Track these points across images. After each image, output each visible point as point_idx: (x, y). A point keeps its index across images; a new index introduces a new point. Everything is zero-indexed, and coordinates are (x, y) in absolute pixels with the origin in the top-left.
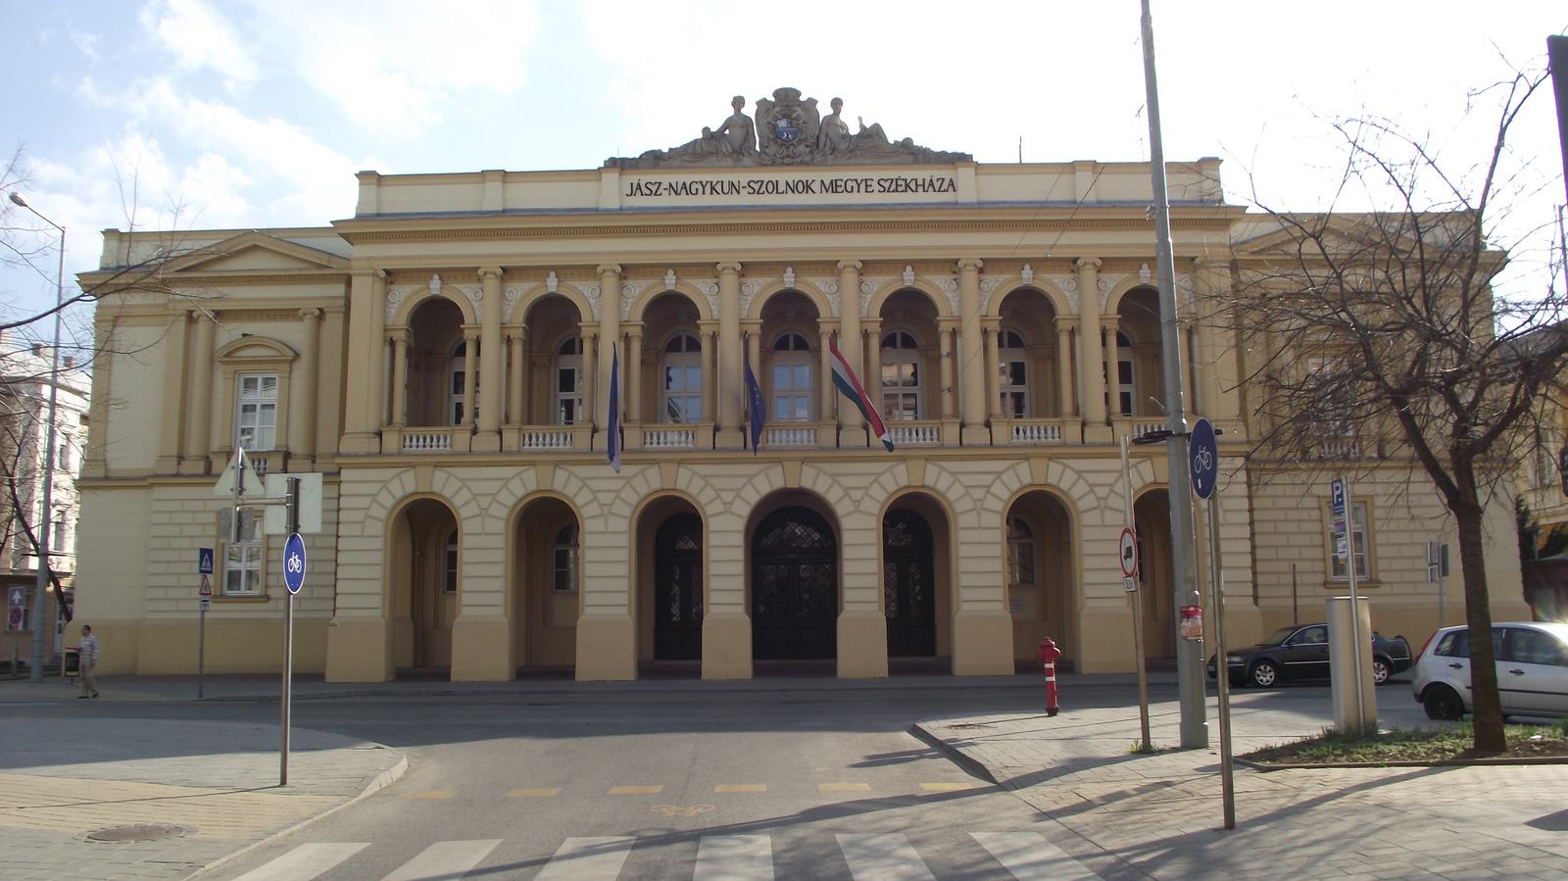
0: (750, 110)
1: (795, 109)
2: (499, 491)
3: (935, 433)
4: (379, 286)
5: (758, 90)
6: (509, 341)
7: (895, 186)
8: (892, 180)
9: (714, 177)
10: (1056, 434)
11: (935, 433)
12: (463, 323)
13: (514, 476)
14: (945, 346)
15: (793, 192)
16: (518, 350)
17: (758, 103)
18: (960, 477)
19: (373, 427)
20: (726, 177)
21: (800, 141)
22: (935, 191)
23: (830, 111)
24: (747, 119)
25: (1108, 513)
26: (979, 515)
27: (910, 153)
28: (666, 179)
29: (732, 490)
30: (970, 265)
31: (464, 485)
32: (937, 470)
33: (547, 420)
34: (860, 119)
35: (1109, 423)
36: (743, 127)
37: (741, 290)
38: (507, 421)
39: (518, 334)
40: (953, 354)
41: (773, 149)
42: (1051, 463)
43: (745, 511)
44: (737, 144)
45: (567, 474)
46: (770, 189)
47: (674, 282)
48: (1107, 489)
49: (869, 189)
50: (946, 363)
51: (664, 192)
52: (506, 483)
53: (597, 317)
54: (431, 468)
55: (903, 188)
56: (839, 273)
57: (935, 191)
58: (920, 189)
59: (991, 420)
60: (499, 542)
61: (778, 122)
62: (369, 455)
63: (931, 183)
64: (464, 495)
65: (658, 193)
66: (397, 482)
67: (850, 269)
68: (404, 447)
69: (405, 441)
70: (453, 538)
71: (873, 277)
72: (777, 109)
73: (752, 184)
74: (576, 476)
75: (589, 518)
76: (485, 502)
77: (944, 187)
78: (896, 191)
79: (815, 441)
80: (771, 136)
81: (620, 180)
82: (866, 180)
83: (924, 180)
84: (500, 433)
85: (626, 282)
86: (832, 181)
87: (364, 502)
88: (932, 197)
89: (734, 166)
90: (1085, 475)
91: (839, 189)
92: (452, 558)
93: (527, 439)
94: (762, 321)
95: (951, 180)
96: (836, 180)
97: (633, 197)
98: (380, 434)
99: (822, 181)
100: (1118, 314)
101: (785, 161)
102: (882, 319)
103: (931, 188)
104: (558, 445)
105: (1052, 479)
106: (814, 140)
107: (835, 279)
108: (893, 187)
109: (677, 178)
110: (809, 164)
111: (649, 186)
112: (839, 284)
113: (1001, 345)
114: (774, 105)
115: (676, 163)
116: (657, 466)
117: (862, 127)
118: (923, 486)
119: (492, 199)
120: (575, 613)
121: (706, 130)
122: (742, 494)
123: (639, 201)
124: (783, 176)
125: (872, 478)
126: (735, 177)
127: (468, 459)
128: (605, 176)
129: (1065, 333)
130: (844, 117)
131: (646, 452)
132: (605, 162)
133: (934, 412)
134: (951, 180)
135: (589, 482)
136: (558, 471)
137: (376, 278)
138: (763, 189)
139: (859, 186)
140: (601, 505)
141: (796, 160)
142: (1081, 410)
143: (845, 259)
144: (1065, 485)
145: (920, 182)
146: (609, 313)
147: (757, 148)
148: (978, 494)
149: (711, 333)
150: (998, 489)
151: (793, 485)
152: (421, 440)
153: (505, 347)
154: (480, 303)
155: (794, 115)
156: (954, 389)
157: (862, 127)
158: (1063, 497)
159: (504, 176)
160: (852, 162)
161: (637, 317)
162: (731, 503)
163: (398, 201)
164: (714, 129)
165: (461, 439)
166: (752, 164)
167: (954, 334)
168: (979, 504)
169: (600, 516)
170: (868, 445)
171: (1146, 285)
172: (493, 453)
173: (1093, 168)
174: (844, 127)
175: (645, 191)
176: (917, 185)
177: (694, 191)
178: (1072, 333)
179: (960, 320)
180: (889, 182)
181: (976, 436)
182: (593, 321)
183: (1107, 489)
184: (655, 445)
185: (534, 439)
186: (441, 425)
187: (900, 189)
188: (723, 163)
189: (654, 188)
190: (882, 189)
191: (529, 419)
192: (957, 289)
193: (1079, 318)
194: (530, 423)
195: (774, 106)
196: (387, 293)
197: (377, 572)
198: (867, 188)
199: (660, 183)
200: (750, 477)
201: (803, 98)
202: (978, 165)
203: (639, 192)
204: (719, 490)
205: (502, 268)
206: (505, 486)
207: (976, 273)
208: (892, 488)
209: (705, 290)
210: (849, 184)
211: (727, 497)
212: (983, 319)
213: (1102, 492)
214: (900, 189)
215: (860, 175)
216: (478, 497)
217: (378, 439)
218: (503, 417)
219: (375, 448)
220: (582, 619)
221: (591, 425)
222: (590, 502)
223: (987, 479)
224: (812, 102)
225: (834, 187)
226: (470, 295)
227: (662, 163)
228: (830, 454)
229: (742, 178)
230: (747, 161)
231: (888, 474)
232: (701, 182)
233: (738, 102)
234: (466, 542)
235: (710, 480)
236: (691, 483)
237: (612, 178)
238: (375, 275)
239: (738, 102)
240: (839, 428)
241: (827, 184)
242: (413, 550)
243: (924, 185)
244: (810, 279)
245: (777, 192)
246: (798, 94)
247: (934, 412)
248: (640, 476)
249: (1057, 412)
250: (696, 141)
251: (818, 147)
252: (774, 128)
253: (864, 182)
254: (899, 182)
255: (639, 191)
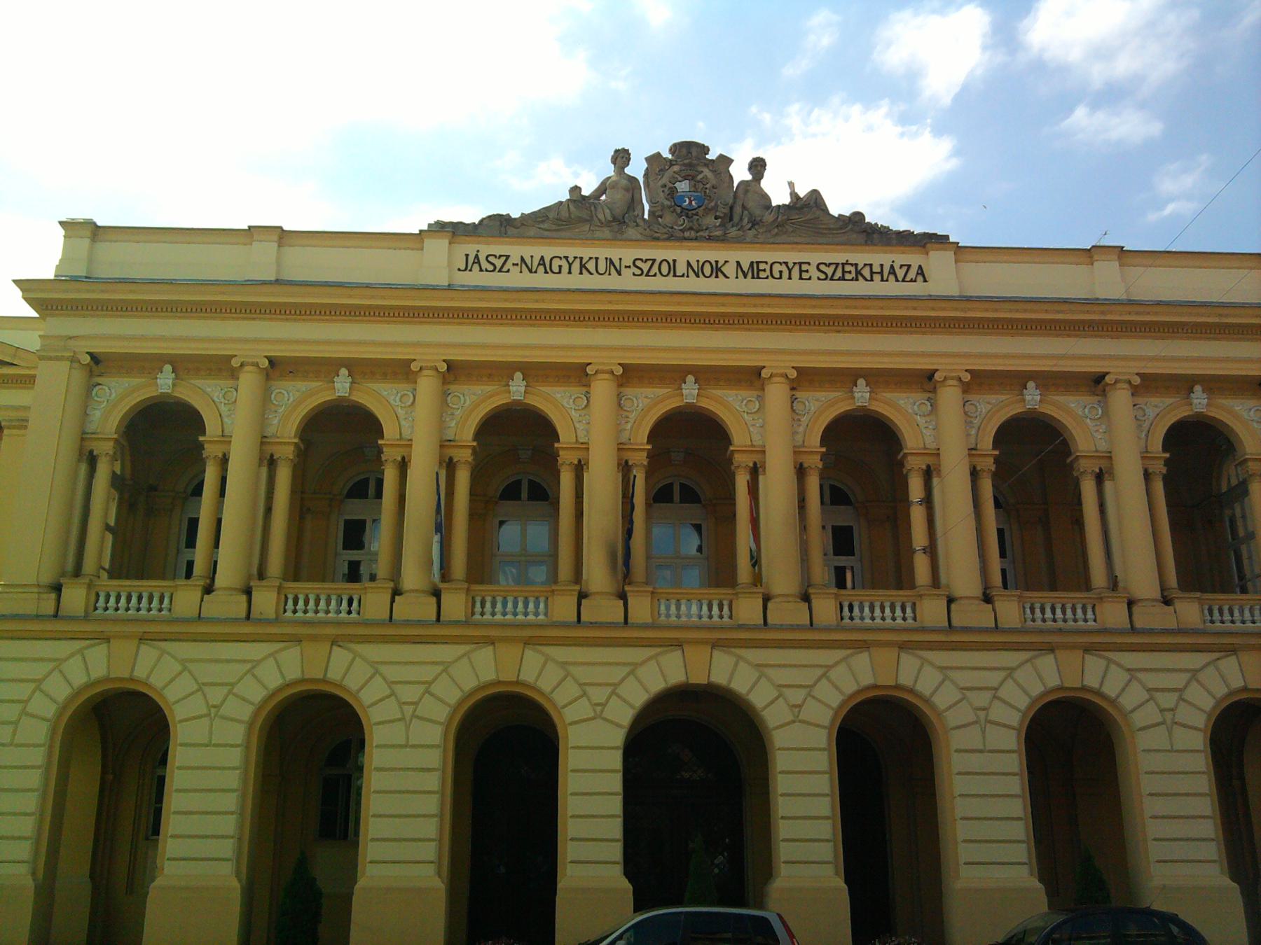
0: (637, 169)
1: (700, 169)
2: (436, 679)
3: (726, 609)
4: (79, 376)
5: (651, 140)
6: (272, 463)
7: (842, 272)
8: (837, 264)
9: (586, 252)
10: (1090, 615)
11: (909, 610)
12: (203, 432)
13: (265, 658)
14: (916, 489)
15: (698, 276)
16: (1159, 487)
17: (648, 159)
18: (952, 674)
19: (47, 578)
20: (603, 252)
21: (708, 211)
22: (897, 280)
23: (749, 177)
24: (633, 180)
25: (1178, 731)
26: (1170, 732)
27: (857, 229)
28: (516, 251)
29: (222, 684)
30: (952, 378)
31: (185, 668)
32: (1103, 663)
33: (321, 575)
34: (791, 185)
35: (987, 599)
36: (627, 190)
37: (620, 405)
38: (261, 576)
39: (464, 456)
40: (928, 501)
41: (668, 219)
42: (903, 655)
43: (625, 717)
44: (618, 212)
45: (542, 659)
46: (665, 269)
47: (523, 389)
48: (1175, 696)
49: (805, 275)
50: (917, 515)
51: (512, 268)
52: (253, 667)
53: (406, 433)
54: (1080, 653)
55: (853, 275)
56: (233, 374)
57: (897, 280)
58: (877, 277)
59: (811, 591)
60: (434, 758)
61: (677, 185)
62: (38, 617)
63: (892, 271)
64: (571, 689)
65: (505, 269)
66: (842, 668)
67: (606, 376)
68: (96, 609)
69: (97, 601)
70: (164, 761)
71: (1146, 399)
72: (676, 168)
73: (639, 263)
74: (364, 659)
75: (777, 728)
76: (215, 695)
77: (912, 275)
78: (842, 279)
79: (731, 617)
80: (667, 203)
81: (449, 250)
82: (800, 264)
83: (882, 266)
84: (248, 592)
85: (452, 387)
86: (752, 263)
87: (23, 691)
88: (892, 288)
89: (615, 239)
90: (1139, 675)
91: (762, 275)
92: (161, 781)
93: (290, 602)
94: (649, 447)
95: (920, 267)
96: (758, 263)
97: (496, 273)
98: (57, 588)
99: (738, 263)
100: (822, 446)
101: (687, 234)
102: (649, 447)
103: (892, 278)
104: (493, 614)
105: (528, 675)
106: (727, 210)
107: (755, 393)
108: (839, 274)
109: (533, 251)
110: (723, 239)
111: (491, 259)
112: (760, 398)
113: (380, 483)
114: (671, 163)
115: (532, 232)
116: (491, 648)
117: (794, 195)
118: (518, 683)
119: (260, 263)
120: (350, 871)
121: (575, 190)
122: (45, 686)
123: (475, 278)
124: (683, 255)
125: (819, 672)
126: (615, 253)
127: (197, 629)
128: (428, 243)
129: (1089, 477)
130: (766, 184)
131: (477, 625)
132: (430, 225)
133: (901, 578)
134: (920, 267)
135: (382, 669)
136: (716, 653)
137: (76, 365)
138: (655, 269)
139: (790, 271)
140: (402, 704)
141: (701, 233)
142: (1121, 585)
143: (771, 365)
144: (1110, 689)
145: (876, 269)
146: (422, 429)
147: (646, 216)
148: (982, 699)
149: (924, 467)
150: (1009, 691)
151: (699, 679)
152: (123, 600)
153: (264, 470)
154: (583, 412)
155: (700, 177)
156: (931, 550)
157: (794, 195)
158: (920, 704)
159: (281, 236)
160: (779, 239)
161: (815, 440)
162: (603, 705)
163: (115, 262)
164: (586, 192)
165: (186, 598)
166: (639, 237)
167: (928, 474)
168: (982, 714)
169: (399, 720)
170: (248, 617)
171: (341, 399)
172: (235, 621)
173: (281, 238)
174: (766, 198)
175: (485, 265)
176: (872, 273)
177: (556, 269)
178: (928, 474)
179: (938, 455)
180: (833, 267)
181: (787, 612)
182: (401, 438)
183: (1175, 696)
184: (488, 617)
185: (301, 603)
186: (164, 578)
187: (848, 276)
188: (598, 234)
189: (499, 263)
190: (823, 276)
191: (294, 571)
192: (931, 411)
193: (937, 454)
194: (296, 578)
195: (671, 165)
196: (90, 388)
197: (230, 802)
198: (801, 275)
199: (508, 257)
200: (634, 667)
201: (712, 156)
202: (957, 248)
203: (476, 267)
204: (585, 684)
205: (270, 362)
206: (1009, 675)
207: (788, 388)
208: (850, 688)
209: (568, 403)
210: (777, 268)
211: (598, 695)
212: (1145, 456)
213: (1168, 700)
214: (848, 276)
215: (792, 257)
216: (206, 689)
217: (53, 596)
218: (255, 571)
219: (48, 606)
220: (361, 883)
221: (391, 585)
222: (388, 697)
223: (993, 678)
224: (725, 161)
225: (754, 271)
226: (217, 396)
227: (511, 231)
228: (942, 638)
229: (625, 254)
230: (631, 232)
231: (1211, 669)
232: (566, 258)
233: (621, 157)
234: (179, 756)
235: (572, 669)
236: (545, 674)
237: (439, 245)
238: (74, 360)
239: (621, 157)
240: (766, 599)
241: (746, 267)
242: (104, 773)
243: (881, 273)
244: (1061, 399)
245: (675, 275)
246: (705, 149)
247: (901, 578)
248: (465, 660)
249: (1084, 583)
250: (561, 203)
251: (731, 219)
252: (673, 191)
253: (797, 267)
254: (848, 268)
255: (476, 266)
